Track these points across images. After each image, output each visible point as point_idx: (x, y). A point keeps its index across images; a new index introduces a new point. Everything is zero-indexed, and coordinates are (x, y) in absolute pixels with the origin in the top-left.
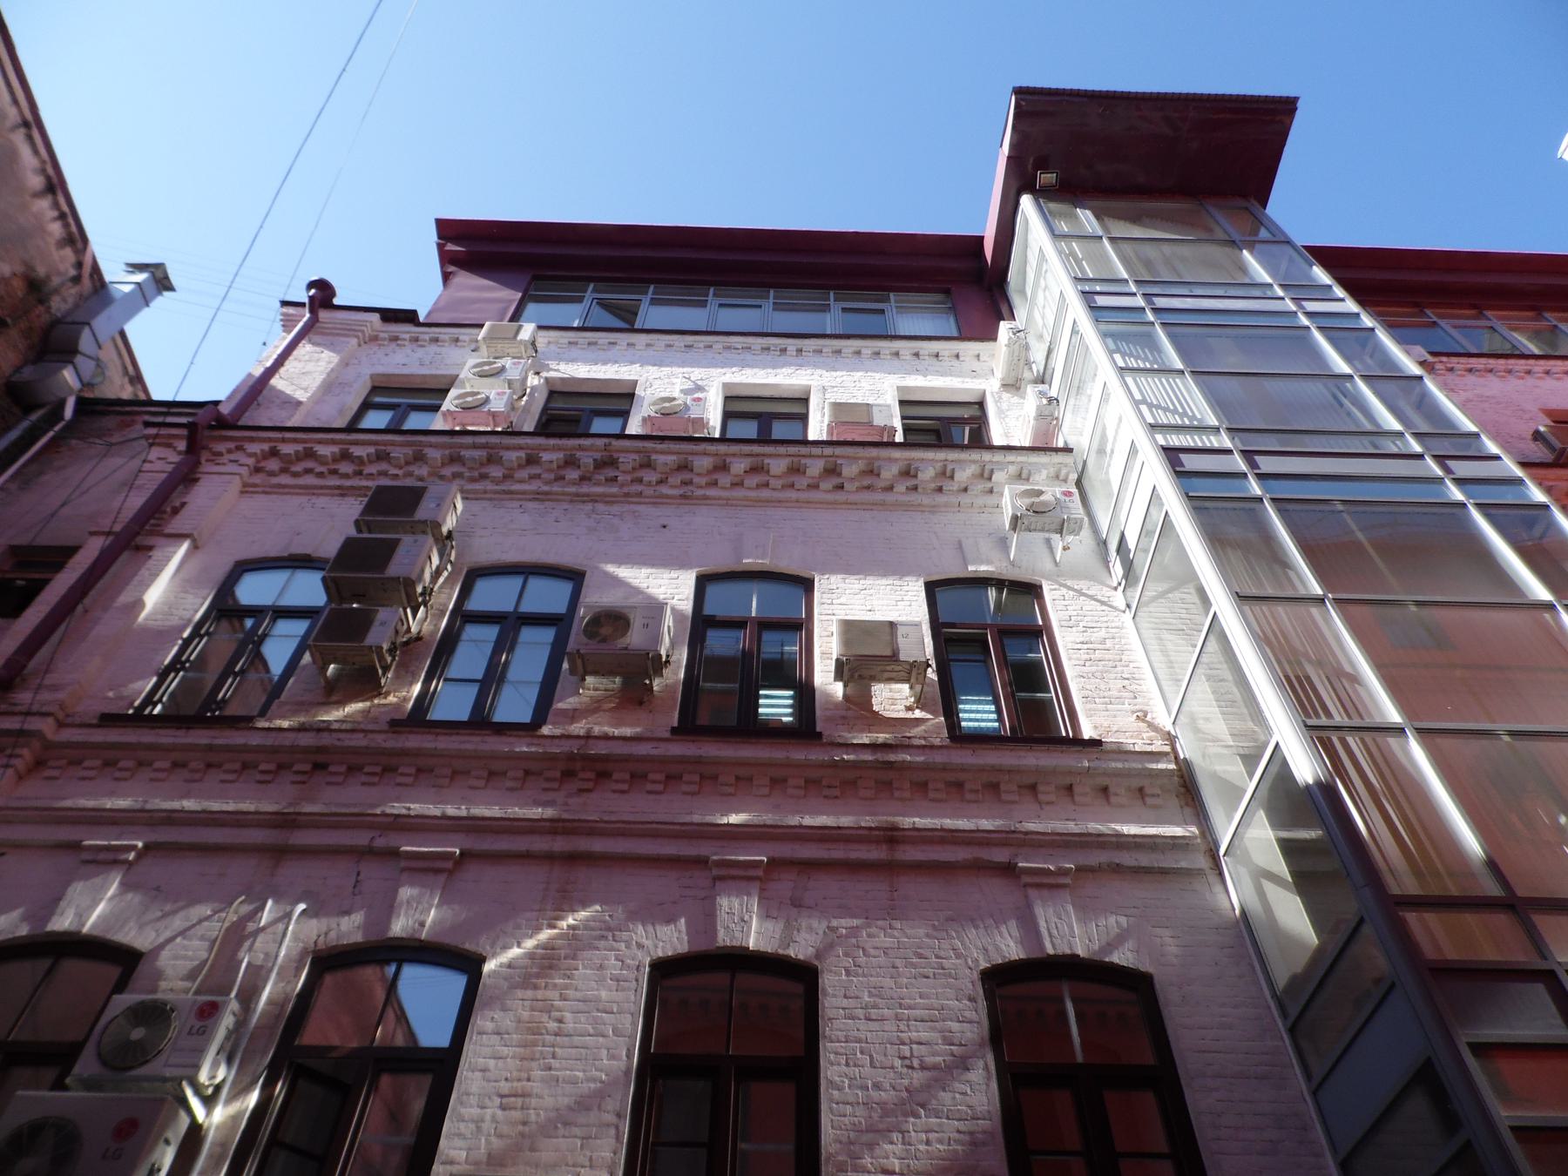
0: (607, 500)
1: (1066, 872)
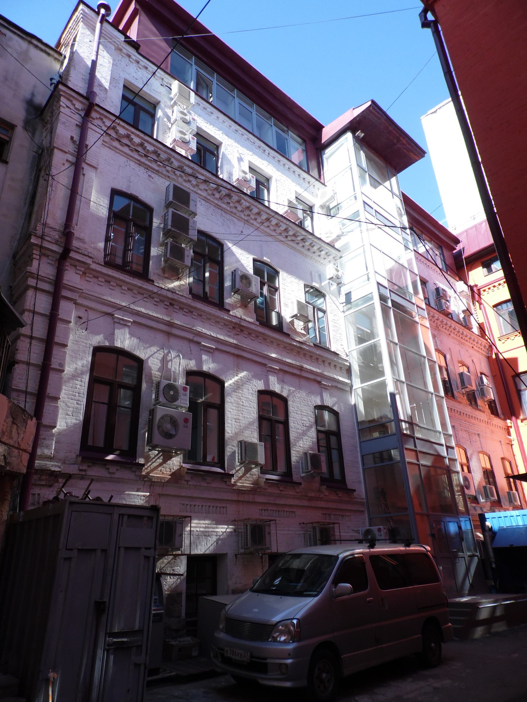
0: (222, 209)
1: (329, 386)
